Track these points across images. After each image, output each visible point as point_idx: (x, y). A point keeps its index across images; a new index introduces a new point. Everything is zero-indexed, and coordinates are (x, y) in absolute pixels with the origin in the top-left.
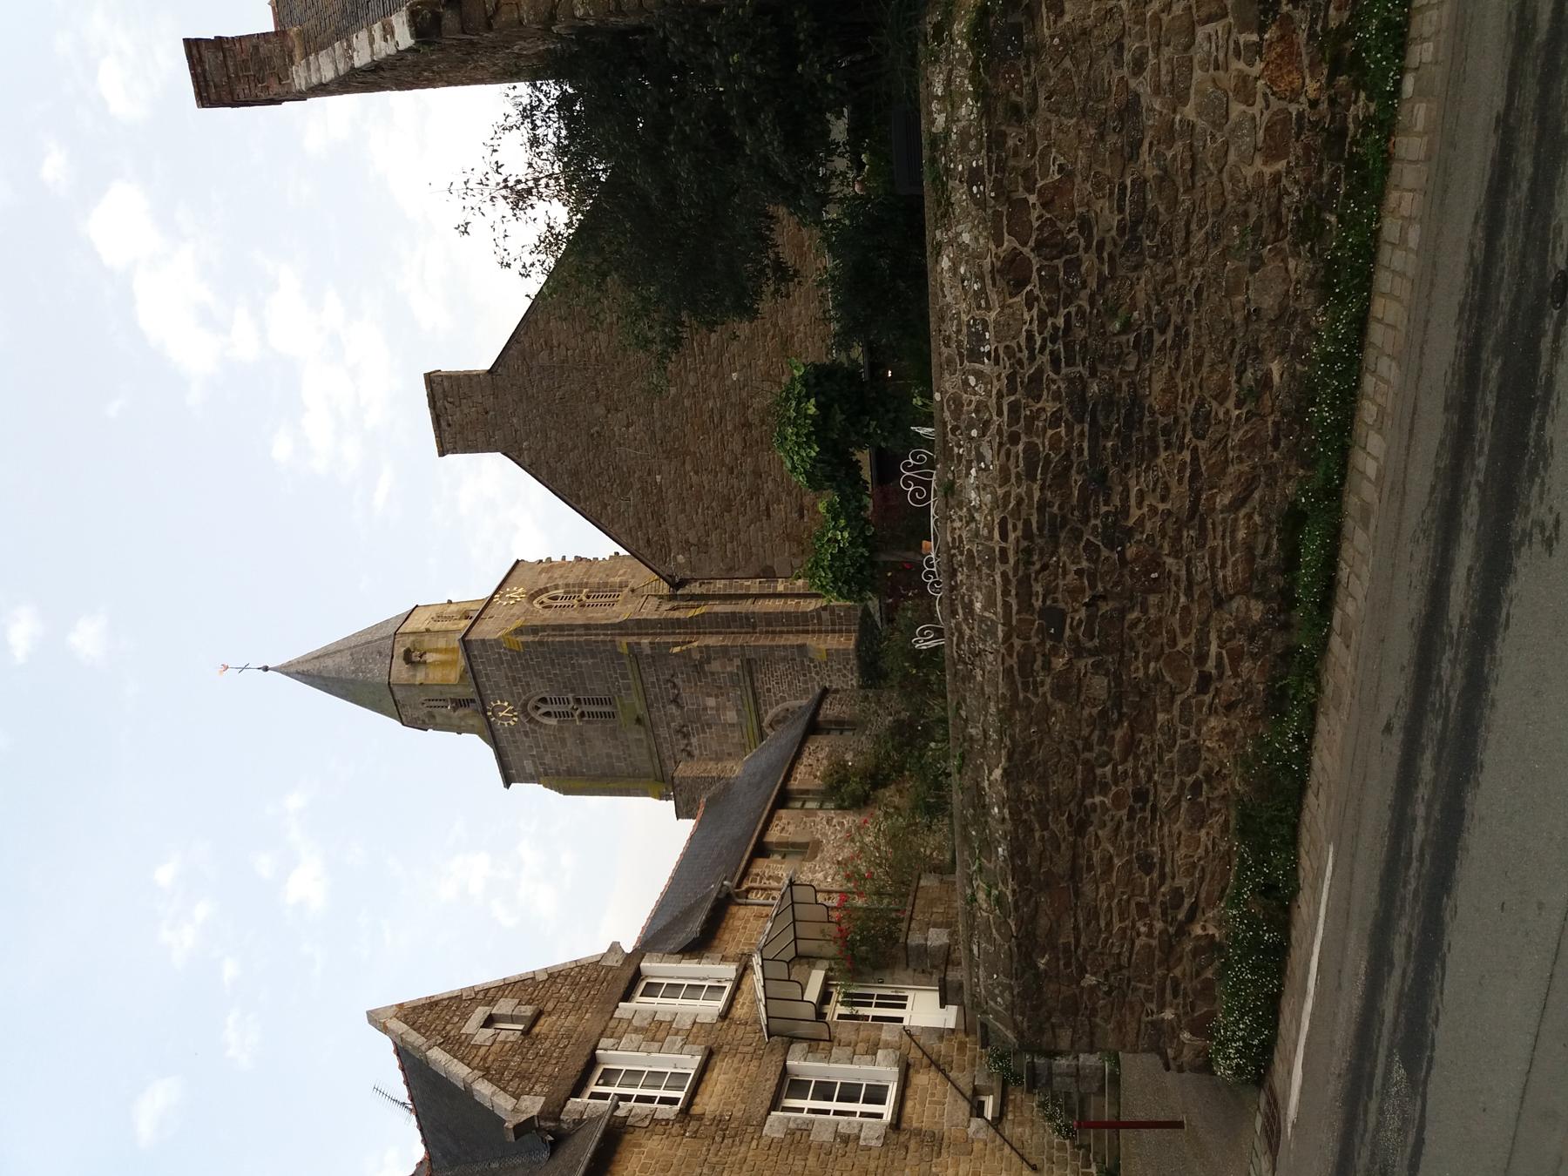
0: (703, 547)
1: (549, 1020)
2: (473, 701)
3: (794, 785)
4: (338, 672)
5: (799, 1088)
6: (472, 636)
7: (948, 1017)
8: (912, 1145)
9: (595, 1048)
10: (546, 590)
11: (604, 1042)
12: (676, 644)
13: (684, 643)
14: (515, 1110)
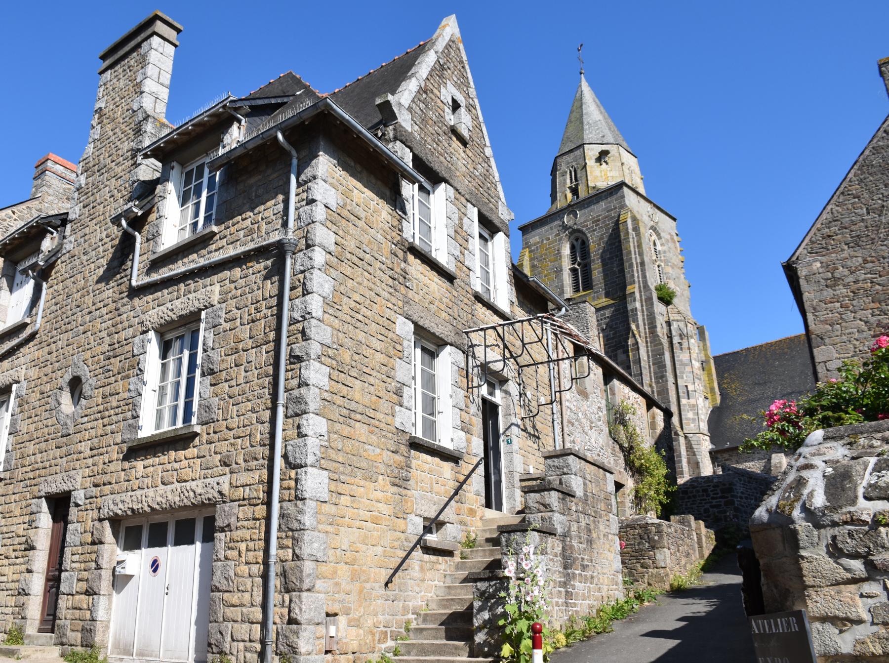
0: (834, 282)
1: (461, 151)
2: (578, 197)
3: (616, 382)
4: (587, 114)
5: (431, 354)
6: (625, 189)
7: (779, 402)
8: (397, 457)
9: (447, 182)
10: (659, 236)
11: (451, 190)
12: (638, 327)
13: (639, 332)
14: (400, 104)
